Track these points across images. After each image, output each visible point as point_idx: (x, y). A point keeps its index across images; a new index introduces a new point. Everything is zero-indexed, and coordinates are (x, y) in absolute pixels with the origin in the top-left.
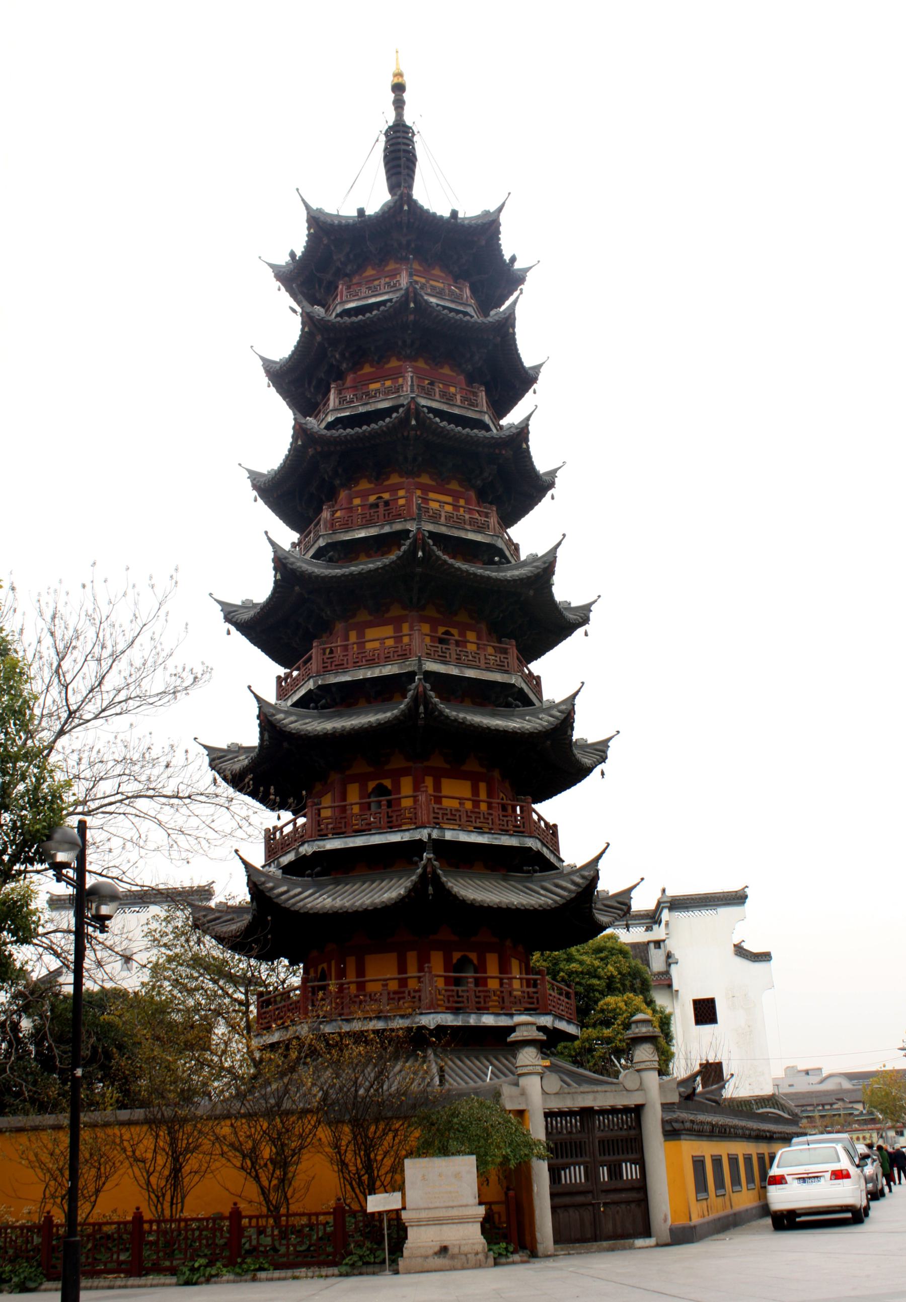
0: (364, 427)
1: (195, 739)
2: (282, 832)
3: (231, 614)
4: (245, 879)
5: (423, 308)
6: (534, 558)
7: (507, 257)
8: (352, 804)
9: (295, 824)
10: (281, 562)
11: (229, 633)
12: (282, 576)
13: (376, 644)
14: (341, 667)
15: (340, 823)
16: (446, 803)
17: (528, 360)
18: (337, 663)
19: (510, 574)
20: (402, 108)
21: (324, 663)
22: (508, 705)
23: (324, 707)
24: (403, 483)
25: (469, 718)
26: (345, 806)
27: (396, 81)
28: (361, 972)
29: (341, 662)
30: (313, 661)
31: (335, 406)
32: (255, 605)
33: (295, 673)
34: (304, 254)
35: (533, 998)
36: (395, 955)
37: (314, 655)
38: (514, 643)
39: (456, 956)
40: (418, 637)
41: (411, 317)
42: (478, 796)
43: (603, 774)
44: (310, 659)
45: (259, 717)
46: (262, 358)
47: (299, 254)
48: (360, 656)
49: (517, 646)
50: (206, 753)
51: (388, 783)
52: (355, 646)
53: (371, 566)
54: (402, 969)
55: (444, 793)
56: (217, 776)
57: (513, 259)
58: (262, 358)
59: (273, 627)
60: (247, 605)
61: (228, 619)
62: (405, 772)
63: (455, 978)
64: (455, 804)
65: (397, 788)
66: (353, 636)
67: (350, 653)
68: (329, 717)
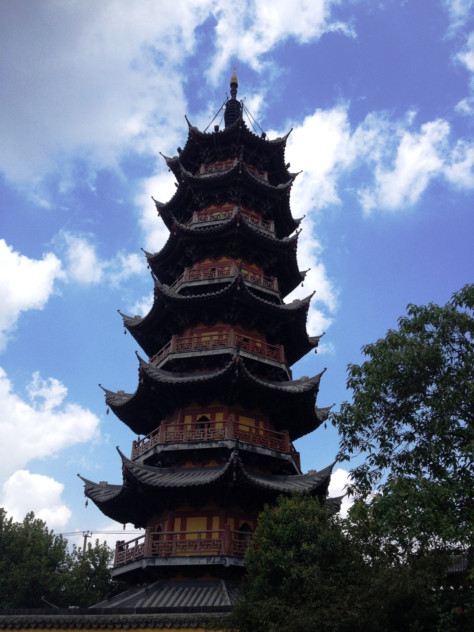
0: (203, 295)
1: (100, 385)
2: (128, 546)
3: (91, 491)
4: (121, 465)
5: (244, 226)
6: (312, 474)
7: (286, 163)
8: (187, 425)
9: (137, 543)
10: (144, 374)
11: (87, 504)
12: (158, 297)
13: (208, 339)
14: (187, 350)
15: (180, 435)
16: (241, 428)
17: (301, 269)
18: (185, 347)
19: (289, 388)
20: (236, 94)
21: (153, 547)
22: (284, 474)
23: (175, 371)
24: (227, 262)
25: (257, 480)
26: (183, 425)
27: (233, 81)
28: (183, 527)
29: (187, 347)
30: (171, 346)
31: (186, 279)
32: (125, 395)
33: (146, 440)
34: (185, 148)
35: (282, 444)
36: (205, 518)
37: (171, 343)
38: (283, 347)
39: (242, 522)
40: (231, 336)
41: (234, 381)
42: (259, 426)
43: (326, 426)
44: (170, 345)
45: (139, 370)
46: (156, 202)
47: (182, 149)
48: (198, 344)
49: (289, 434)
50: (85, 484)
51: (208, 416)
52: (178, 535)
53: (201, 377)
54: (209, 526)
55: (241, 422)
56: (127, 330)
57: (289, 165)
58: (156, 202)
59: (148, 333)
60: (121, 394)
61: (126, 325)
62: (219, 410)
63: (240, 534)
64: (247, 429)
65: (213, 418)
66: (178, 522)
67: (193, 342)
68: (177, 377)
